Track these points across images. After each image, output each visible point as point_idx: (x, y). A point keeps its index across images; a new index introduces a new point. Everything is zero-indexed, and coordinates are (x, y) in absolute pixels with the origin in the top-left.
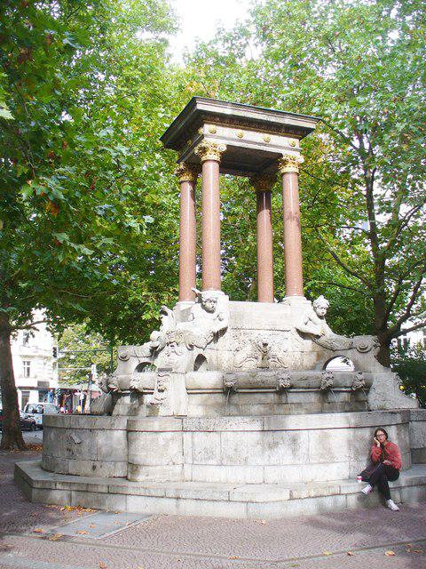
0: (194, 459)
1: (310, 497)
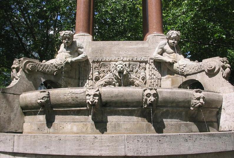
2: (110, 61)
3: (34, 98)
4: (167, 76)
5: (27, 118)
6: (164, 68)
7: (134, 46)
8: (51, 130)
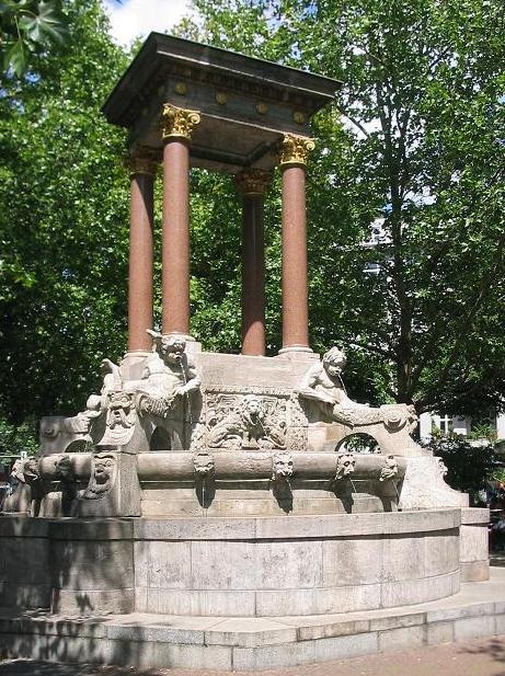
0: (150, 581)
1: (326, 637)
2: (234, 393)
5: (149, 493)
6: (315, 409)
7: (271, 369)
8: (210, 510)
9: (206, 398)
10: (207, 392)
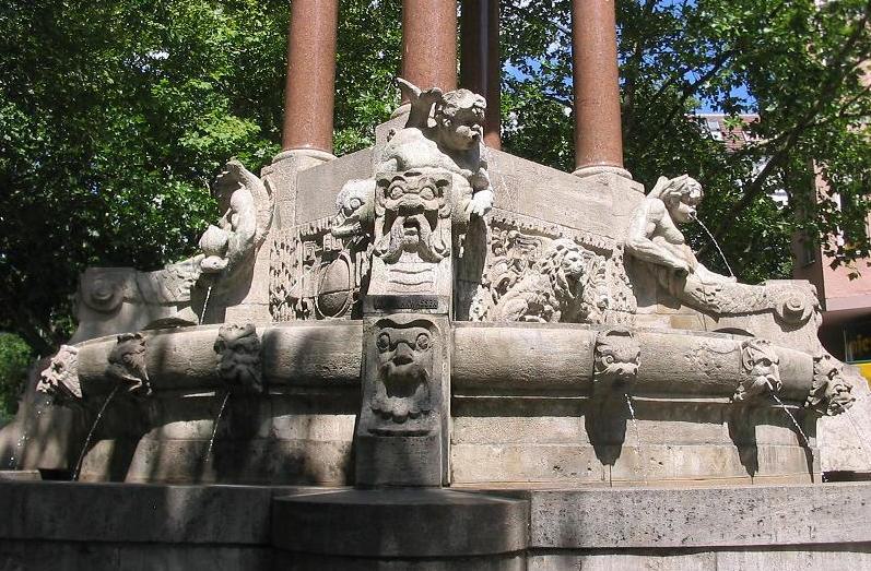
2: (535, 232)
3: (561, 349)
4: (654, 307)
5: (462, 420)
7: (584, 197)
8: (618, 470)
9: (490, 235)
10: (494, 224)
